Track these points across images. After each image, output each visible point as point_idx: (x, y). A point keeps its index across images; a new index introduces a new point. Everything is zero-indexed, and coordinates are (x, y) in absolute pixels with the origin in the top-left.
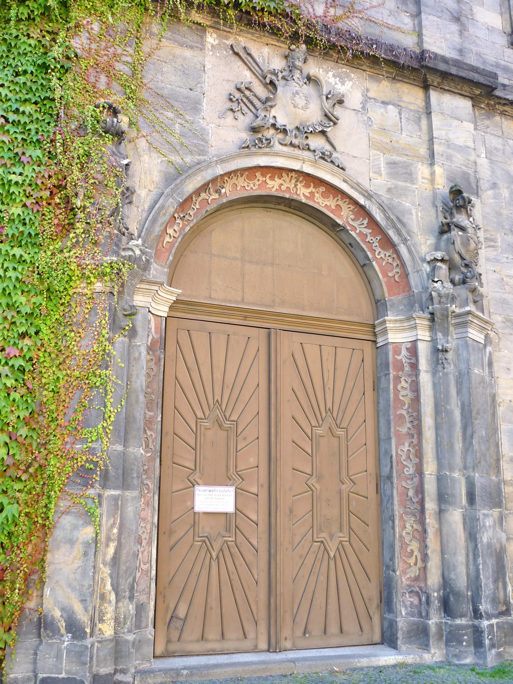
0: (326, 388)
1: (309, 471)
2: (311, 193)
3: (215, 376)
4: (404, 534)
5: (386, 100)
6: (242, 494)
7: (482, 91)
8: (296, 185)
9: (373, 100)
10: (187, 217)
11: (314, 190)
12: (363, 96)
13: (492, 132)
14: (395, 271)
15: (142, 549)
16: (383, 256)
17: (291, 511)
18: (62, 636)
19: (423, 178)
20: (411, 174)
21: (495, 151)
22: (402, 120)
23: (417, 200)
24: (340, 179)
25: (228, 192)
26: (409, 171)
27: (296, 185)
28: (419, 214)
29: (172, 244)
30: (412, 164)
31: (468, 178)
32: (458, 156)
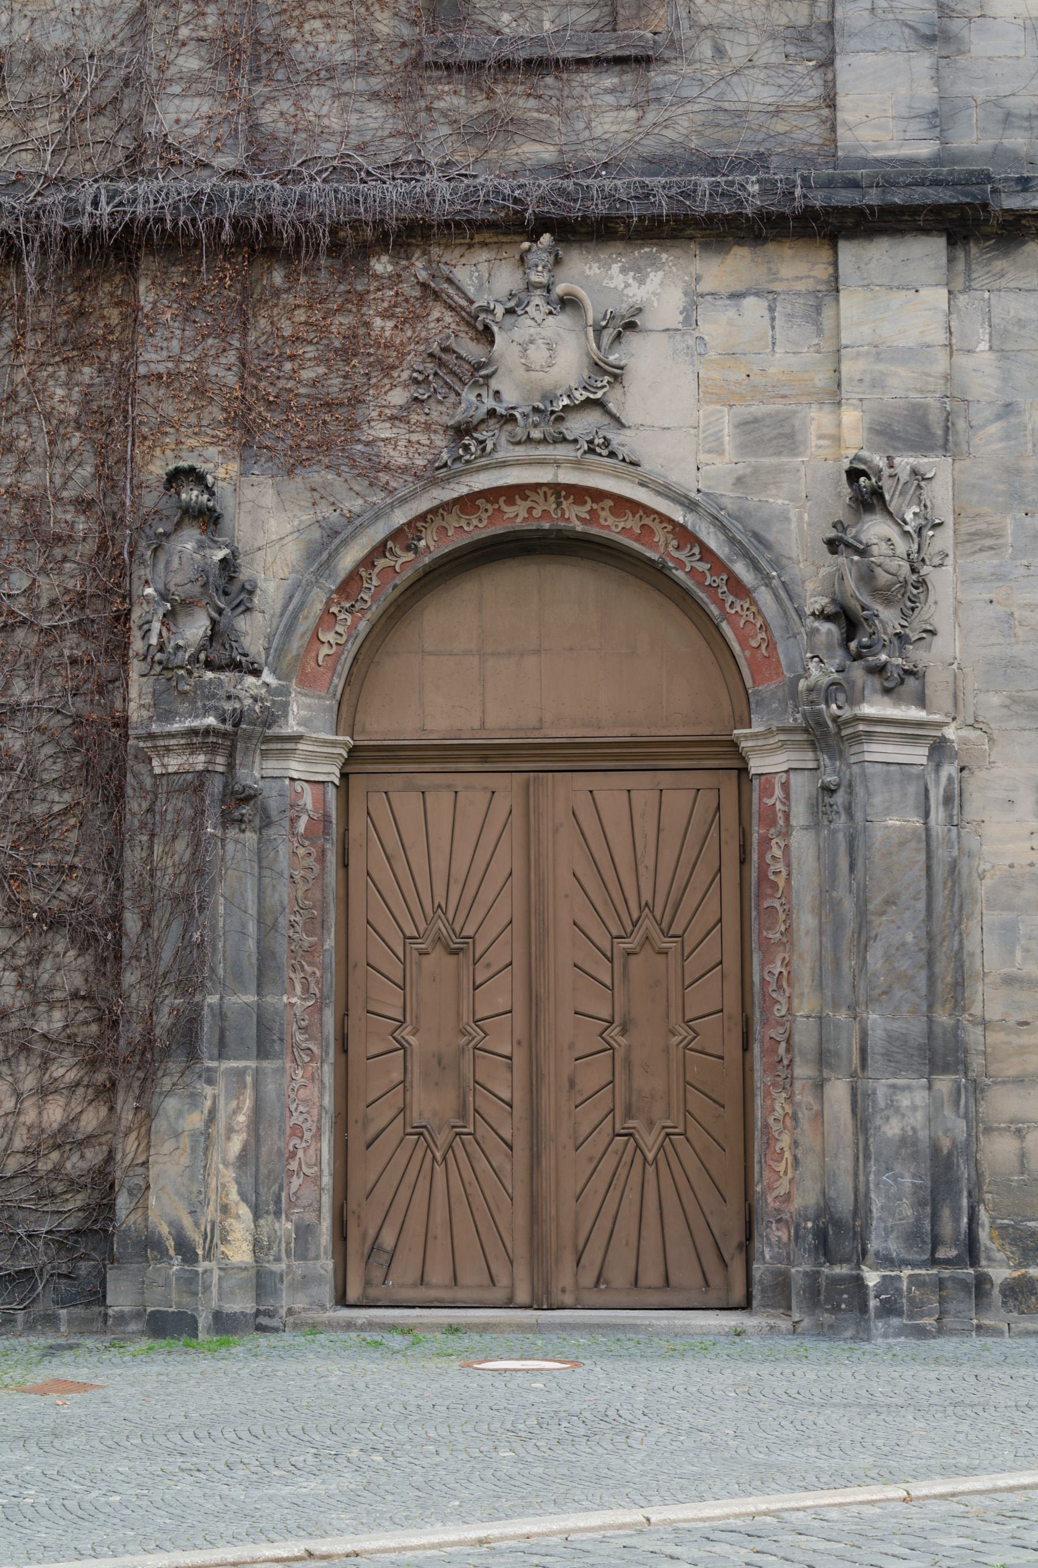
0: (641, 868)
1: (605, 1014)
2: (591, 512)
3: (433, 865)
4: (771, 1121)
5: (739, 287)
6: (484, 1057)
7: (963, 216)
8: (559, 504)
9: (709, 298)
10: (358, 606)
11: (595, 506)
12: (686, 294)
13: (1012, 285)
14: (760, 636)
15: (304, 1145)
16: (739, 609)
17: (572, 1084)
18: (171, 1258)
19: (820, 437)
20: (791, 436)
21: (1016, 329)
22: (777, 323)
23: (803, 487)
24: (633, 482)
25: (432, 544)
26: (787, 430)
27: (559, 504)
28: (806, 516)
29: (337, 656)
30: (795, 412)
31: (925, 415)
32: (901, 371)
